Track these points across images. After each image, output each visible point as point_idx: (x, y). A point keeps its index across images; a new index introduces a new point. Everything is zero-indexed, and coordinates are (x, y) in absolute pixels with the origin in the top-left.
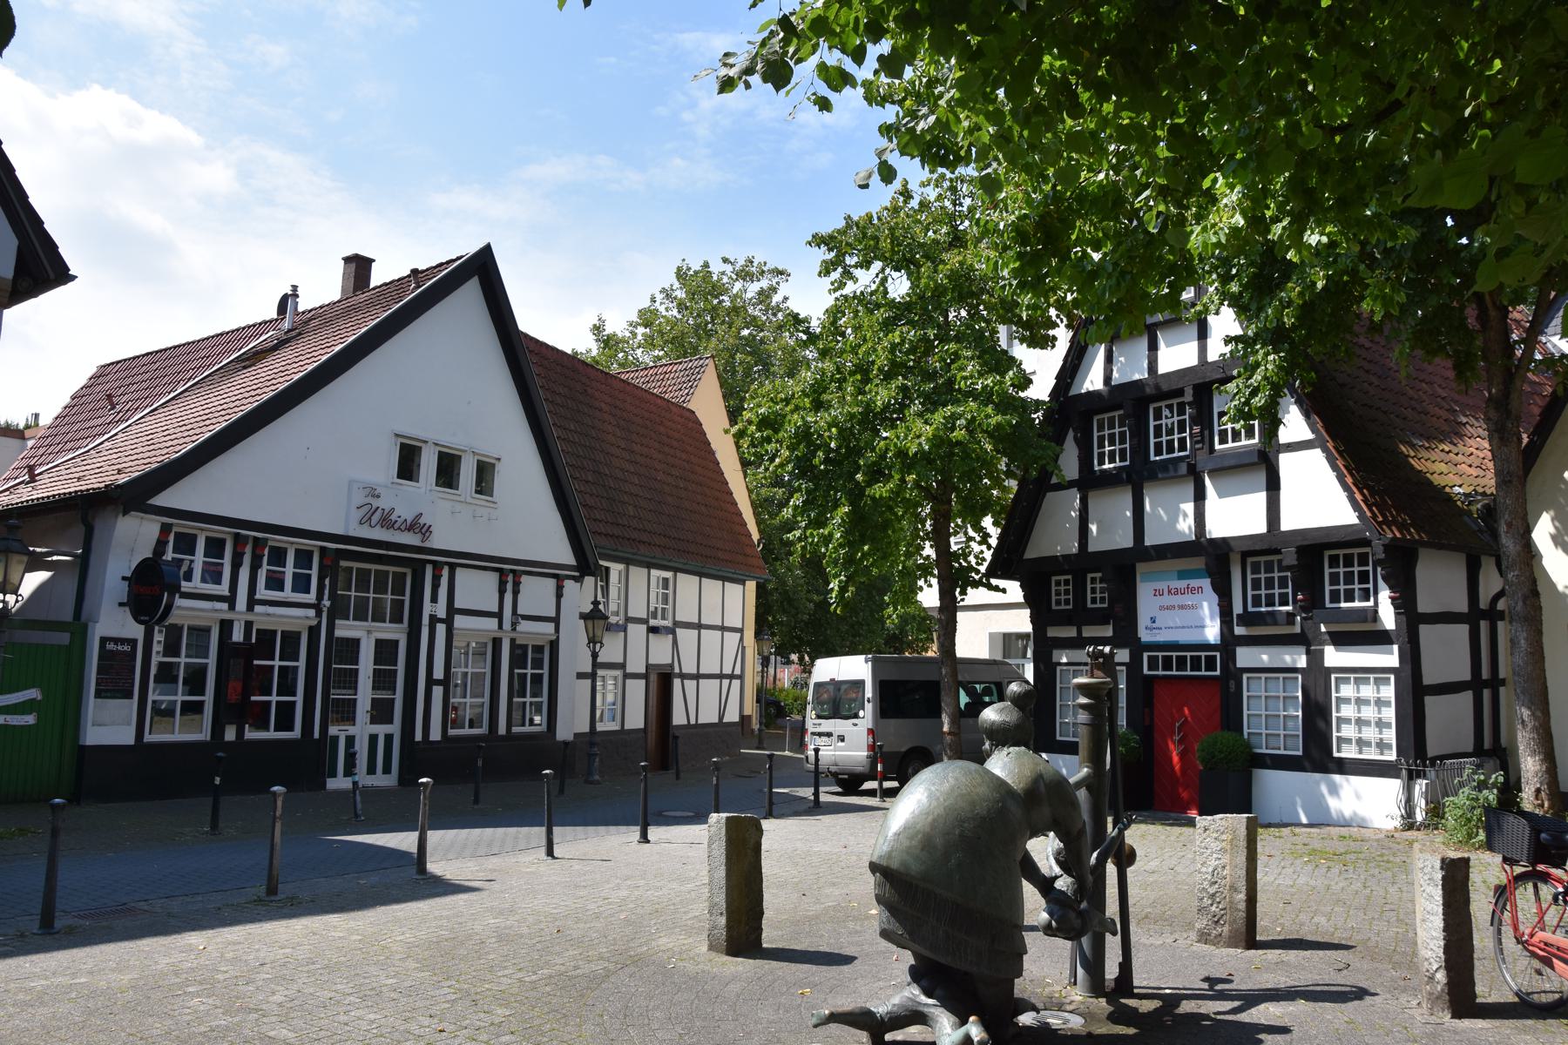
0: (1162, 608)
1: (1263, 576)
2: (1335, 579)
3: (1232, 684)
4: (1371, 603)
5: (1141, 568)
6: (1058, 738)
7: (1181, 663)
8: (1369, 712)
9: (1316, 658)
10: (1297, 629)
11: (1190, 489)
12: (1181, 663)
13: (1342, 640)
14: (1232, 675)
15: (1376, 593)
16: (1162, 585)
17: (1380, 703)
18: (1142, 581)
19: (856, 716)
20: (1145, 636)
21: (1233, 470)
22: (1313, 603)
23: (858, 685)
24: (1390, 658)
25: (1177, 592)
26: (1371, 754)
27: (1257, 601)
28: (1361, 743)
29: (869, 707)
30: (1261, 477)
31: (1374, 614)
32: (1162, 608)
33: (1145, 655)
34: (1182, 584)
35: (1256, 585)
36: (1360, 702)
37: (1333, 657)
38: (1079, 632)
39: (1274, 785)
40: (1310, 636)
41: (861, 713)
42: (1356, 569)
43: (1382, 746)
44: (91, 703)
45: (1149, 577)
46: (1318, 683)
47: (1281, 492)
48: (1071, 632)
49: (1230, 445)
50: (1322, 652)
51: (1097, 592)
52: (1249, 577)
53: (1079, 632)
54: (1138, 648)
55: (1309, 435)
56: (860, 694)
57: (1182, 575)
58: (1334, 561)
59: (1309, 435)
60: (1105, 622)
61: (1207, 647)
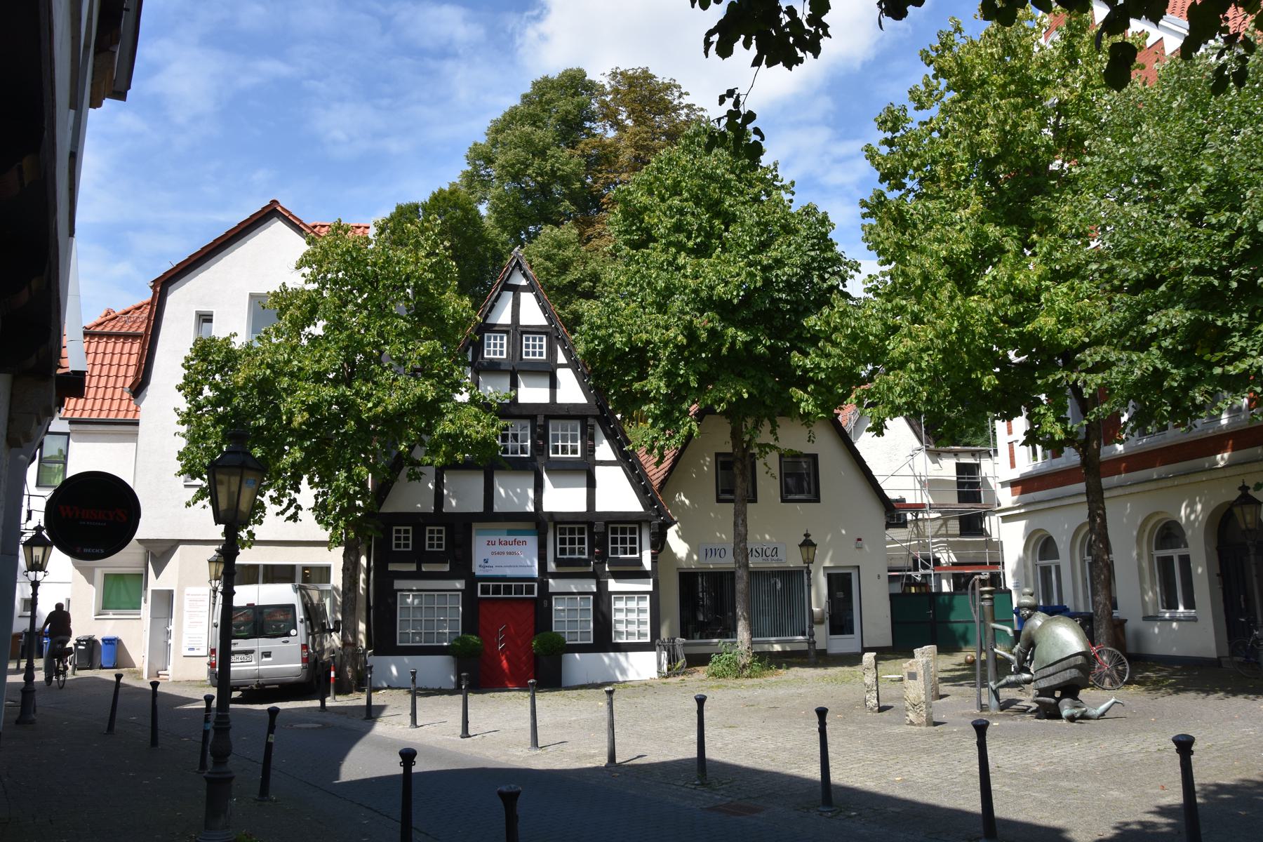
0: (493, 553)
1: (619, 536)
2: (614, 541)
3: (546, 603)
4: (638, 555)
5: (475, 526)
6: (398, 644)
7: (508, 590)
8: (633, 616)
9: (602, 586)
10: (591, 569)
11: (531, 480)
12: (497, 590)
13: (618, 576)
14: (546, 595)
15: (641, 551)
16: (495, 538)
17: (640, 611)
18: (477, 534)
19: (288, 635)
20: (478, 570)
21: (564, 470)
22: (603, 558)
23: (290, 608)
24: (648, 587)
25: (506, 543)
26: (635, 640)
27: (563, 551)
28: (629, 634)
29: (301, 627)
30: (584, 479)
31: (639, 562)
32: (493, 553)
33: (479, 584)
34: (511, 538)
35: (563, 541)
36: (629, 611)
37: (613, 585)
38: (419, 567)
39: (579, 664)
40: (599, 573)
41: (293, 632)
42: (628, 536)
43: (640, 635)
44: (641, 569)
45: (483, 532)
46: (602, 602)
47: (597, 490)
48: (412, 568)
49: (560, 455)
50: (607, 582)
51: (435, 539)
52: (558, 537)
53: (419, 567)
54: (472, 580)
55: (614, 458)
56: (290, 617)
57: (510, 533)
58: (614, 531)
59: (614, 458)
60: (444, 561)
61: (532, 579)
